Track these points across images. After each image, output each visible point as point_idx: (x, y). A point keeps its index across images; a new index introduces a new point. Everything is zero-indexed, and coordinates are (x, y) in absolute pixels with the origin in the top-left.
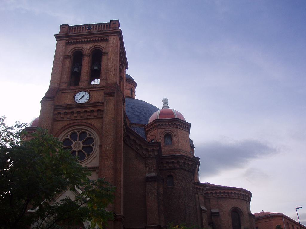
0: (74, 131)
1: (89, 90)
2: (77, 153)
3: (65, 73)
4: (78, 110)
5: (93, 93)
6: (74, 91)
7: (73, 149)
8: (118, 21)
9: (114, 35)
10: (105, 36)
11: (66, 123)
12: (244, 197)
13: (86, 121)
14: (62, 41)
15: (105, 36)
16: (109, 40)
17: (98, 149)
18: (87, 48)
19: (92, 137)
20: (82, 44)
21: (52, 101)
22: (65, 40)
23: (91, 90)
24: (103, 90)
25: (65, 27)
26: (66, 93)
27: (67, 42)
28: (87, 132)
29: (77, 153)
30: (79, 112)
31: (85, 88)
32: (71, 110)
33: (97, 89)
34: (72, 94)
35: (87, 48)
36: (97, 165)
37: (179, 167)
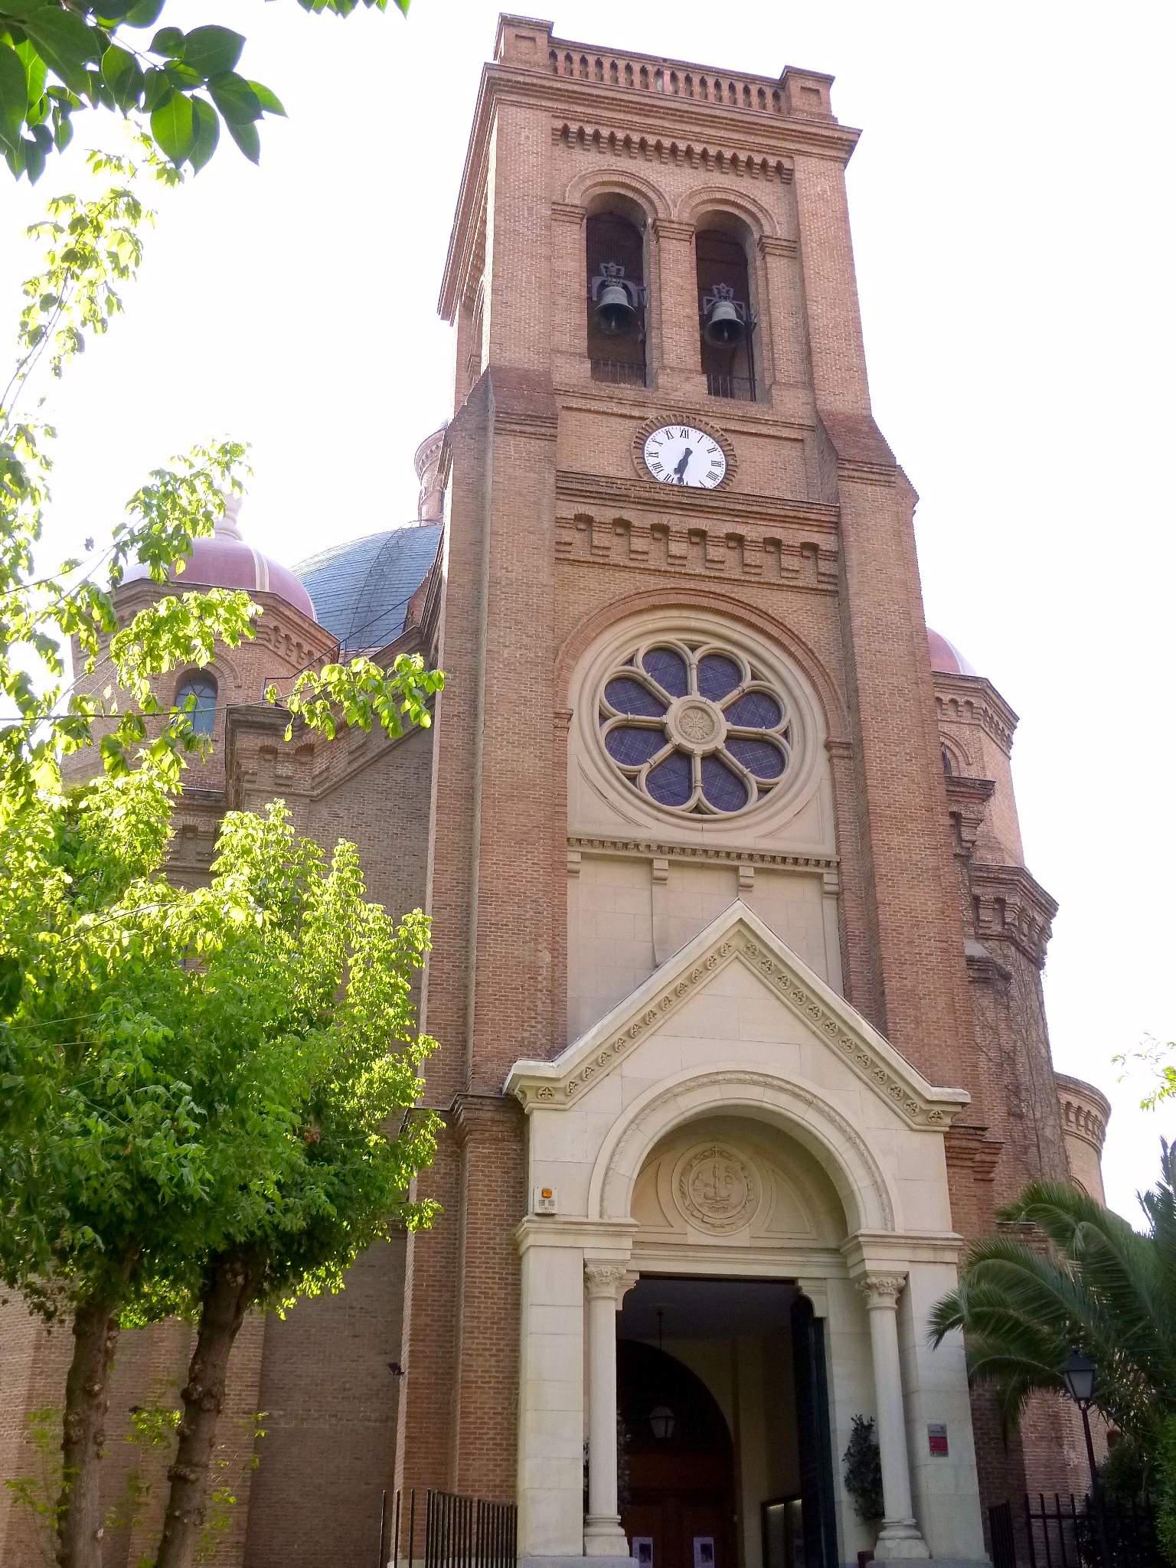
0: (735, 650)
1: (718, 424)
2: (667, 750)
3: (562, 301)
4: (583, 509)
5: (743, 448)
6: (636, 413)
7: (677, 739)
8: (828, 80)
9: (823, 157)
10: (774, 151)
11: (623, 584)
12: (1072, 1117)
13: (740, 593)
14: (529, 114)
15: (774, 151)
16: (798, 175)
17: (572, 703)
18: (676, 192)
19: (777, 687)
20: (656, 164)
21: (542, 443)
22: (547, 109)
23: (732, 426)
24: (795, 440)
25: (533, 39)
26: (591, 416)
27: (559, 124)
28: (744, 658)
29: (667, 750)
30: (699, 536)
31: (697, 412)
32: (654, 519)
33: (764, 430)
34: (628, 428)
35: (676, 192)
36: (826, 848)
37: (999, 928)
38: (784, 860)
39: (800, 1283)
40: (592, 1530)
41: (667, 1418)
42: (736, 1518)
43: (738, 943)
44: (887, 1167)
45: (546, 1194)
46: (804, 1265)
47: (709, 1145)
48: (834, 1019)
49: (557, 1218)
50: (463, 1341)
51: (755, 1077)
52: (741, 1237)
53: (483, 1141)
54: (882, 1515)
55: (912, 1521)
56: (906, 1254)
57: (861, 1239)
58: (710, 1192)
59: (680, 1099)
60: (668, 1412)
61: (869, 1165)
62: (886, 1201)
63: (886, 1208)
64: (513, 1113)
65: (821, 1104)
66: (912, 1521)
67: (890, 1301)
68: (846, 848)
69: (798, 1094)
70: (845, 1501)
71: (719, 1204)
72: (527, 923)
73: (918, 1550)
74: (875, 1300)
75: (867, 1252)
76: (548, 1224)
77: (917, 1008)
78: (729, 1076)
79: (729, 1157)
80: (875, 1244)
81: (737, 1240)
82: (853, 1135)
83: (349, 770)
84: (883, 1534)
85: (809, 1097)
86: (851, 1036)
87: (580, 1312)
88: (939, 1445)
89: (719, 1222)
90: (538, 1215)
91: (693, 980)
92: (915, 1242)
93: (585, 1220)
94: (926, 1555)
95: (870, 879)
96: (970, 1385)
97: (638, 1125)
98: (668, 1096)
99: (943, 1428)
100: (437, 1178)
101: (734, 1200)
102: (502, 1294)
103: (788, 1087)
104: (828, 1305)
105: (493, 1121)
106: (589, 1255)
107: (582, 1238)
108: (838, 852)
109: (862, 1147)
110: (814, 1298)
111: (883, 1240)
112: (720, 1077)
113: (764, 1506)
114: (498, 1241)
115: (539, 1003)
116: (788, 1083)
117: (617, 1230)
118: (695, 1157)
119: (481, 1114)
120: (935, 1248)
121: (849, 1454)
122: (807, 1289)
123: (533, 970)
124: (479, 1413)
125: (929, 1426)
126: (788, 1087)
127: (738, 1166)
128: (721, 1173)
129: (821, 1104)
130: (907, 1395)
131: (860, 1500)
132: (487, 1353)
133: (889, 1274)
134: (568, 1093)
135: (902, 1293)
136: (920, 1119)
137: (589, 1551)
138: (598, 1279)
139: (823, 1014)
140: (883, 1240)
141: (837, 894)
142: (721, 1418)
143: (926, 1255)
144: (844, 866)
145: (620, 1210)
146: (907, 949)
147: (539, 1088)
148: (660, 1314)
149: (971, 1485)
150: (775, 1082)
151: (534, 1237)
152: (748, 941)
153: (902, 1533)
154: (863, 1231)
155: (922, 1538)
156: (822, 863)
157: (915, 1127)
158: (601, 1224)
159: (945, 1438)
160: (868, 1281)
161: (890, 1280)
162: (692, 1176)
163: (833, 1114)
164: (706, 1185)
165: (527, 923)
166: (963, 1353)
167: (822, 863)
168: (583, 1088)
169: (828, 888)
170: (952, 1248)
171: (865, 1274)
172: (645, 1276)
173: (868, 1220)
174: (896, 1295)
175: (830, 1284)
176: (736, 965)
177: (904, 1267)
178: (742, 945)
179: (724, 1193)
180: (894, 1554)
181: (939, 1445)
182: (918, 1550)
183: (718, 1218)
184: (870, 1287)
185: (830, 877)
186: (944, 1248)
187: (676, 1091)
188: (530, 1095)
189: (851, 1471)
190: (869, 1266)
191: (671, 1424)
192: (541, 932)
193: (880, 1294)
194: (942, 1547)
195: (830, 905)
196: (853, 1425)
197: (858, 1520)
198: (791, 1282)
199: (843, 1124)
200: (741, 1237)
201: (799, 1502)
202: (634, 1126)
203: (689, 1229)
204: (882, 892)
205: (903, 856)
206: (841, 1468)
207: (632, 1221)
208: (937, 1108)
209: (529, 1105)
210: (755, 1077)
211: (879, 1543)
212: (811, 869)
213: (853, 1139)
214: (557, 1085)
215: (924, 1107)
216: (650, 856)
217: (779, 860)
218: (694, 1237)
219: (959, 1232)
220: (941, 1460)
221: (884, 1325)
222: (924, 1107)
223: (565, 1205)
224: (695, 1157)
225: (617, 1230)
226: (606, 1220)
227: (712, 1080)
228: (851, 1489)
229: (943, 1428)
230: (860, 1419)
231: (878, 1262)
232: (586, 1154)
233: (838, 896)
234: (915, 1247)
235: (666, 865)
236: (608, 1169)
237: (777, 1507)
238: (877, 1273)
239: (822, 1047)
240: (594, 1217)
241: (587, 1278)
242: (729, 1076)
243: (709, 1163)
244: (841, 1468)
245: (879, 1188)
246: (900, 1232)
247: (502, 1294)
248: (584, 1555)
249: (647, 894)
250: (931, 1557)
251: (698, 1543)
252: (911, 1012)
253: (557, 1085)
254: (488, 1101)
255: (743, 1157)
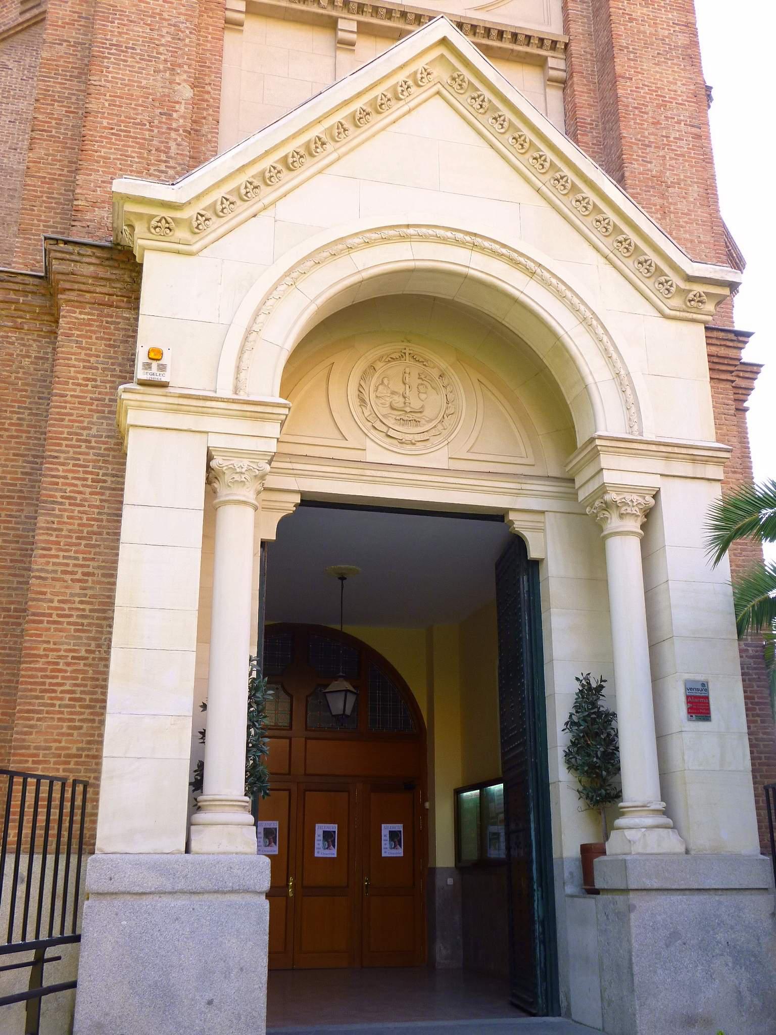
36: (553, 28)
38: (501, 34)
39: (512, 516)
40: (200, 817)
41: (347, 691)
42: (427, 805)
43: (440, 73)
44: (634, 360)
45: (156, 355)
46: (517, 494)
47: (399, 346)
48: (566, 171)
49: (170, 390)
50: (38, 563)
51: (460, 236)
52: (438, 458)
53: (81, 304)
54: (618, 796)
55: (661, 805)
56: (659, 466)
57: (598, 442)
58: (398, 401)
59: (355, 255)
60: (347, 686)
61: (609, 353)
62: (631, 399)
63: (631, 406)
64: (124, 263)
65: (547, 275)
66: (661, 805)
67: (634, 525)
68: (577, 28)
69: (515, 260)
70: (563, 784)
71: (410, 417)
72: (161, 49)
73: (670, 843)
74: (614, 523)
75: (605, 460)
76: (154, 396)
77: (663, 196)
78: (424, 231)
79: (423, 362)
80: (617, 451)
81: (430, 453)
82: (588, 314)
83: (21, 20)
84: (620, 822)
85: (530, 264)
86: (588, 192)
87: (198, 519)
88: (699, 707)
89: (409, 437)
90: (142, 383)
91: (378, 107)
92: (669, 450)
93: (212, 394)
94: (682, 849)
95: (605, 56)
96: (740, 632)
97: (295, 281)
98: (340, 248)
99: (704, 685)
100: (26, 362)
101: (428, 413)
102: (96, 500)
103: (504, 251)
104: (548, 545)
105: (96, 278)
106: (215, 442)
107: (206, 419)
108: (566, 30)
109: (600, 331)
110: (528, 535)
111: (628, 445)
112: (411, 231)
113: (458, 792)
114: (94, 432)
115: (172, 144)
116: (504, 246)
117: (255, 411)
118: (380, 359)
119: (78, 268)
120: (694, 459)
121: (571, 724)
122: (520, 523)
123: (167, 105)
124: (52, 656)
125: (686, 682)
126: (504, 251)
127: (435, 373)
128: (414, 380)
129: (547, 275)
130: (654, 646)
131: (584, 779)
132: (68, 577)
133: (633, 489)
134: (196, 230)
135: (649, 516)
136: (676, 302)
137: (194, 846)
138: (227, 478)
139: (552, 164)
140: (628, 445)
141: (564, 82)
142: (420, 717)
143: (686, 469)
144: (573, 47)
145: (265, 383)
146: (652, 130)
147: (152, 217)
148: (342, 578)
149: (740, 758)
150: (487, 244)
151: (138, 412)
152: (455, 69)
153: (649, 821)
154: (599, 433)
155: (674, 827)
156: (548, 43)
157: (667, 311)
158: (234, 401)
159: (707, 698)
160: (607, 497)
161: (635, 497)
162: (374, 381)
163: (562, 287)
164: (393, 393)
165: (161, 49)
166: (730, 590)
167: (548, 43)
168: (217, 226)
169: (552, 73)
170: (718, 461)
171: (603, 489)
172: (309, 502)
173: (607, 418)
174: (641, 520)
175: (550, 519)
176: (438, 101)
177: (655, 482)
178: (446, 78)
179: (415, 404)
180: (638, 848)
181: (699, 707)
182: (670, 843)
183: (409, 431)
184: (608, 506)
185: (556, 62)
186: (706, 460)
187: (350, 242)
188: (140, 228)
189: (573, 744)
190: (608, 477)
191: (351, 699)
192: (180, 61)
193: (622, 516)
194: (701, 840)
195: (555, 96)
196: (577, 686)
197: (581, 804)
198: (498, 517)
199: (576, 300)
200: (438, 458)
201: (499, 788)
202: (288, 280)
203: (369, 443)
204: (621, 64)
205: (648, 30)
206: (559, 739)
207: (282, 401)
208: (698, 288)
209: (141, 241)
210: (460, 236)
211: (613, 834)
212: (533, 50)
213: (589, 321)
214: (178, 215)
215: (683, 285)
216: (334, 13)
217: (494, 33)
218: (374, 454)
219: (722, 442)
220: (702, 726)
221: (625, 555)
222: (683, 285)
223: (182, 374)
224: (380, 359)
225: (255, 411)
226: (242, 396)
227: (402, 233)
228: (571, 767)
229: (704, 685)
230: (586, 679)
231: (620, 473)
232: (221, 309)
233: (564, 84)
234: (668, 457)
235: (354, 27)
236: (249, 332)
237: (472, 795)
238: (621, 488)
239: (549, 209)
240: (226, 392)
241: (212, 476)
242: (424, 231)
243: (396, 369)
244: (559, 739)
245: (623, 382)
246: (647, 436)
247: (96, 500)
248: (187, 851)
249: (329, 61)
250: (687, 852)
251: (386, 829)
252: (659, 201)
253: (178, 215)
254: (89, 251)
255: (443, 365)
